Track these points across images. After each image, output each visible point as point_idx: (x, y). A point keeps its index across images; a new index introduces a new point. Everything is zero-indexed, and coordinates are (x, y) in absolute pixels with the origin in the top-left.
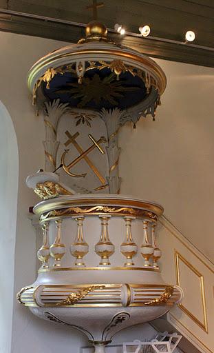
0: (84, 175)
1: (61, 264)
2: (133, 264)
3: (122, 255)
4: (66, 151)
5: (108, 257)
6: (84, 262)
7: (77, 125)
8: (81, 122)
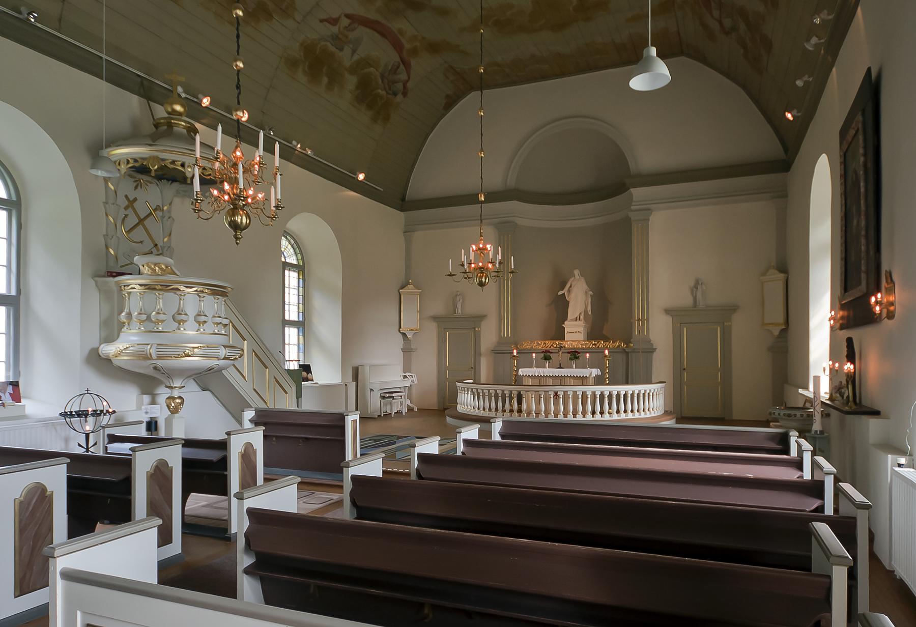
0: (141, 242)
1: (163, 329)
2: (204, 330)
3: (212, 324)
4: (126, 216)
5: (203, 325)
6: (186, 328)
7: (135, 190)
8: (134, 180)
